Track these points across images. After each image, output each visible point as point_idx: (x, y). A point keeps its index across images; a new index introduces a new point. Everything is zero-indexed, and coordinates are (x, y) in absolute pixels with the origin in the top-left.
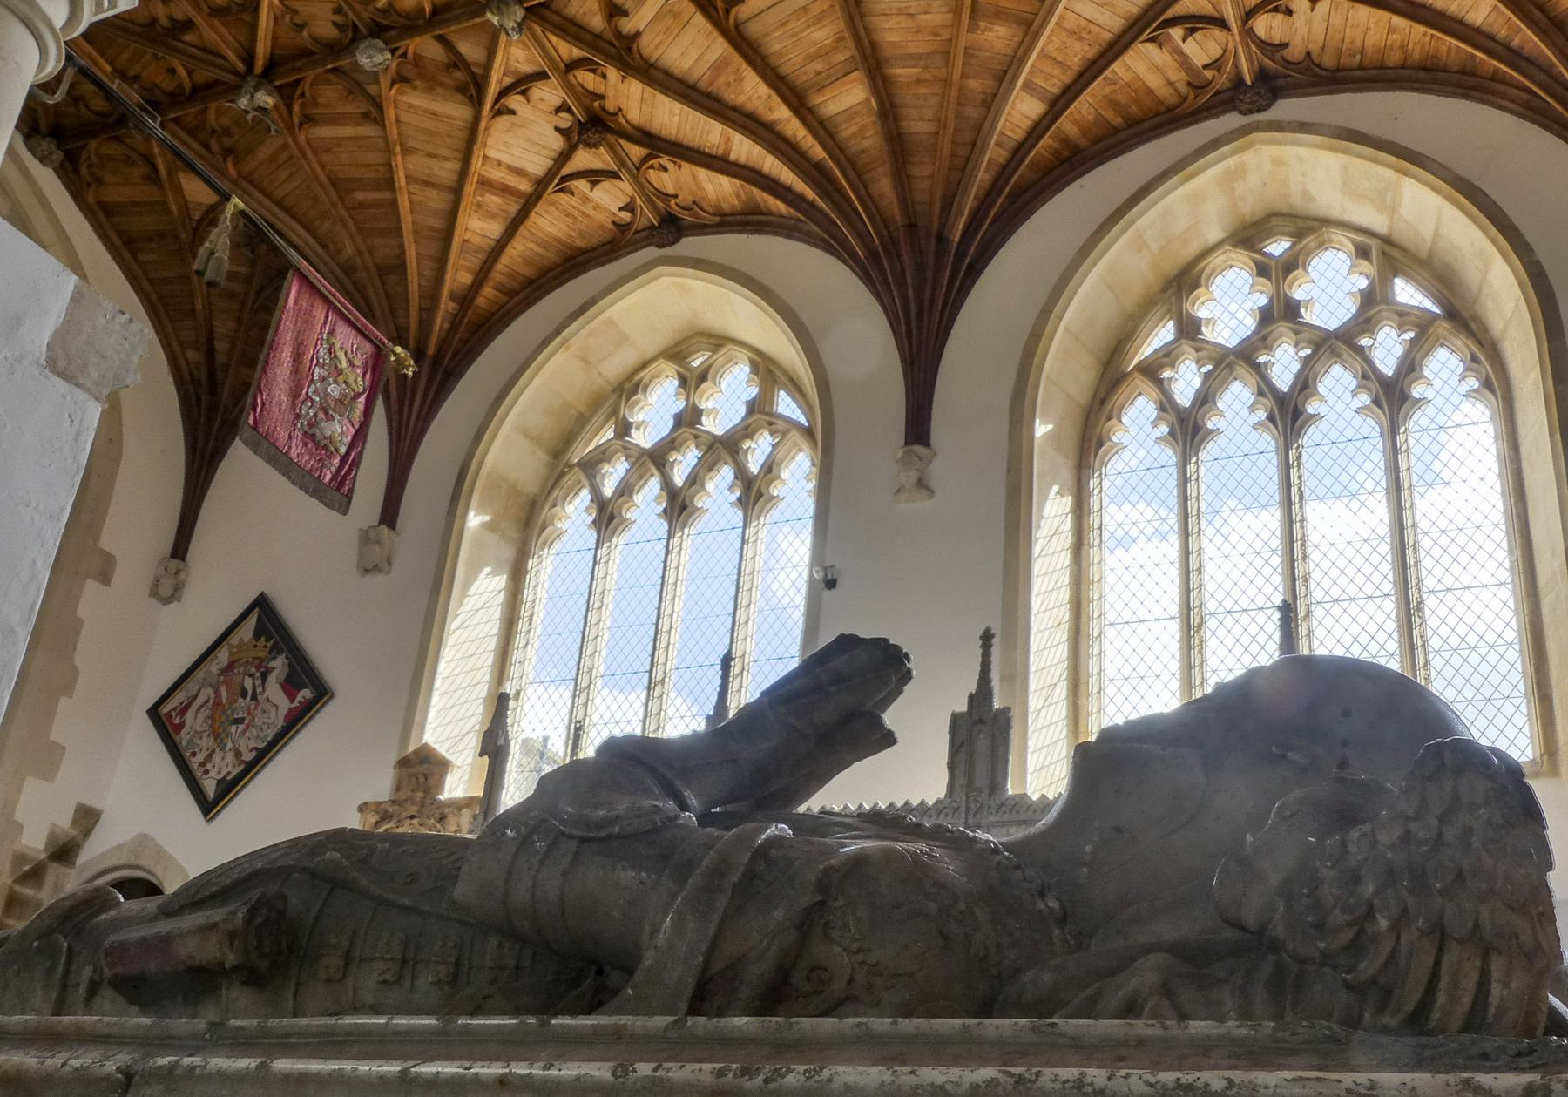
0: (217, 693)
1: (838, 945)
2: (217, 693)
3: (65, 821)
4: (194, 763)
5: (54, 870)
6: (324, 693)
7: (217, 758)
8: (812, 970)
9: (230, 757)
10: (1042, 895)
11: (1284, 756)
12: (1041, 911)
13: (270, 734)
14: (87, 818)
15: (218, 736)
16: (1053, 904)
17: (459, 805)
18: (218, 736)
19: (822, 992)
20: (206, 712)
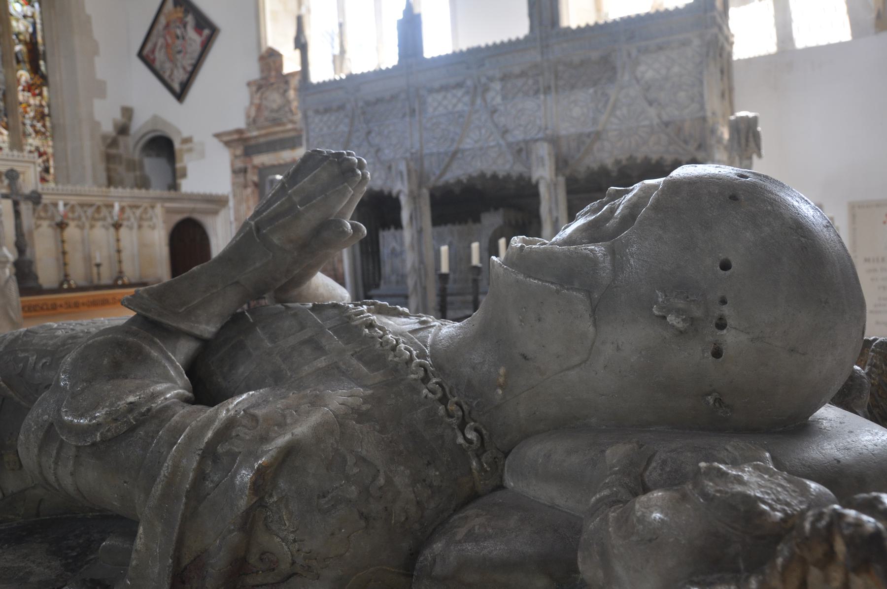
0: (166, 40)
1: (278, 536)
2: (166, 40)
3: (118, 116)
4: (166, 76)
5: (122, 140)
6: (214, 31)
7: (175, 72)
8: (263, 554)
9: (181, 71)
10: (462, 427)
11: (664, 318)
12: (461, 445)
13: (196, 55)
14: (128, 112)
15: (172, 60)
16: (471, 435)
17: (292, 75)
18: (172, 60)
19: (274, 569)
20: (163, 51)
